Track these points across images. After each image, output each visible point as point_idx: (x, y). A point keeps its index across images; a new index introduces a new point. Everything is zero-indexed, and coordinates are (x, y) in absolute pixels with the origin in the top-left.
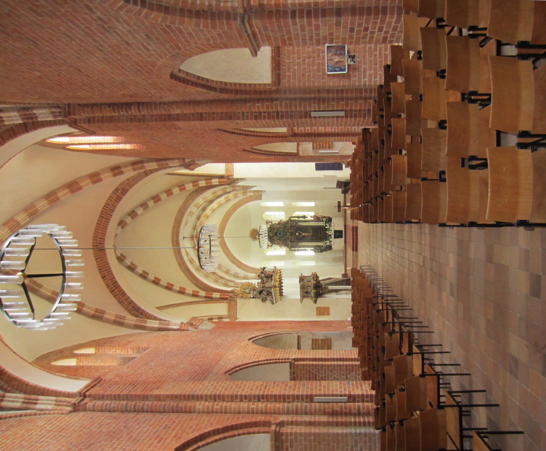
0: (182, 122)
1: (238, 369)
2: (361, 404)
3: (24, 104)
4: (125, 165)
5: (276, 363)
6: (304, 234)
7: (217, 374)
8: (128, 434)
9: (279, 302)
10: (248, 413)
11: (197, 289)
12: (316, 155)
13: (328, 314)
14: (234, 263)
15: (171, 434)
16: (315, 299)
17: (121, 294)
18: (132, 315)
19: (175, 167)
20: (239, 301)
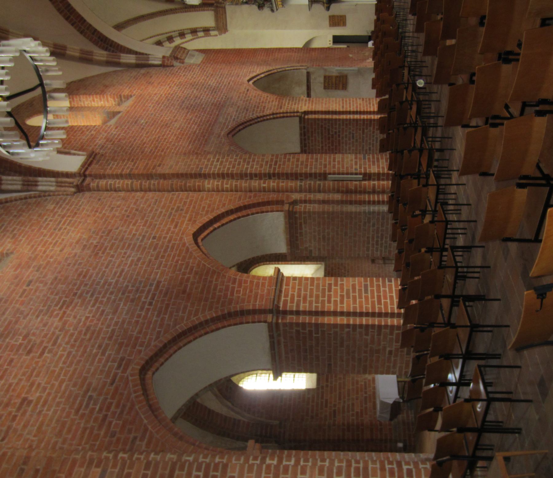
1: (241, 127)
2: (376, 182)
5: (283, 117)
7: (219, 136)
8: (143, 219)
9: (281, 9)
10: (260, 191)
13: (344, 24)
15: (185, 217)
16: (327, 5)
18: (99, 47)
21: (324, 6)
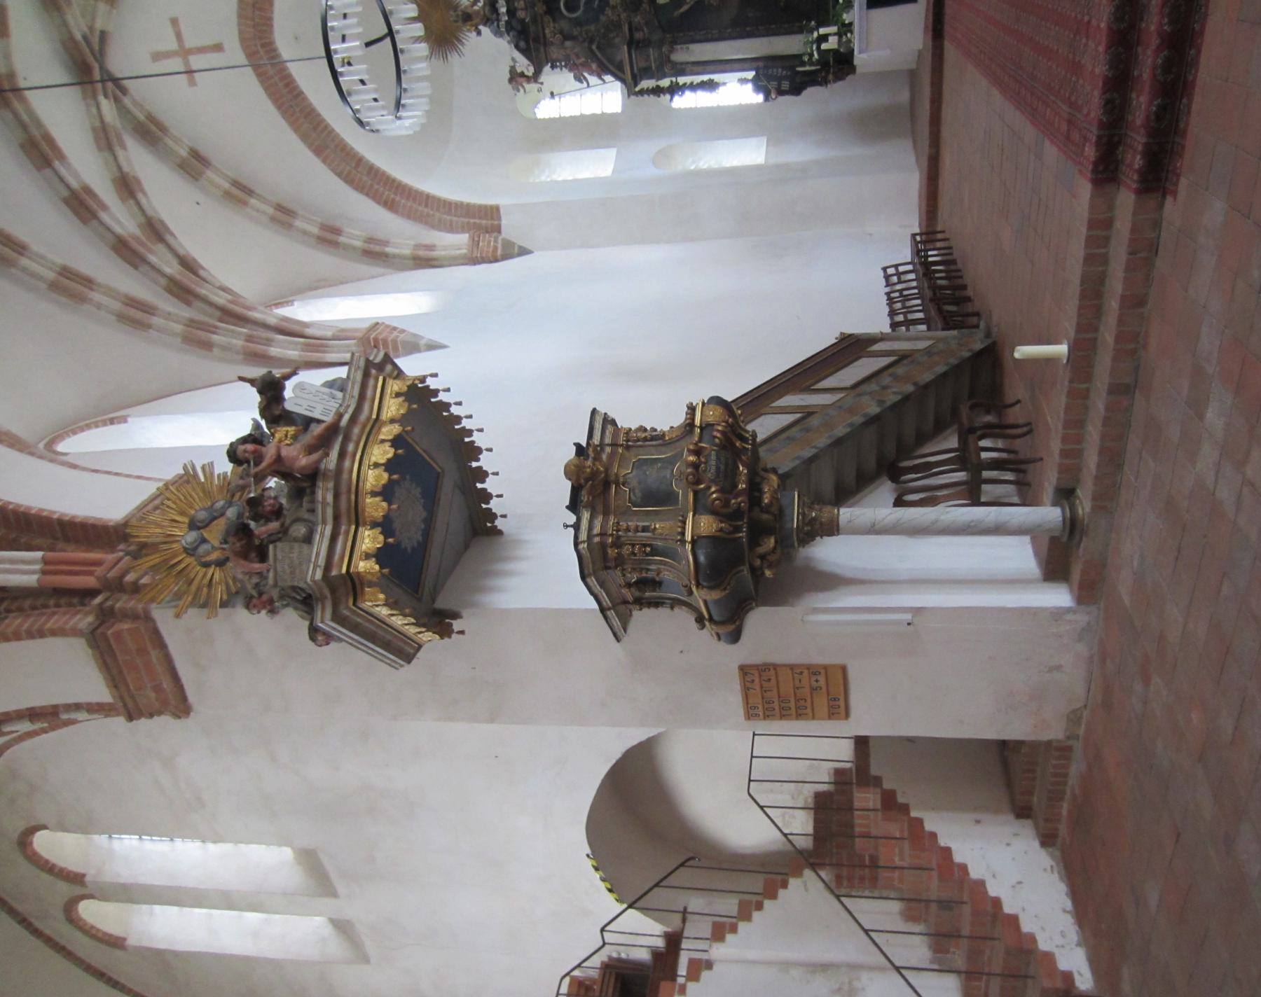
14: (360, 188)
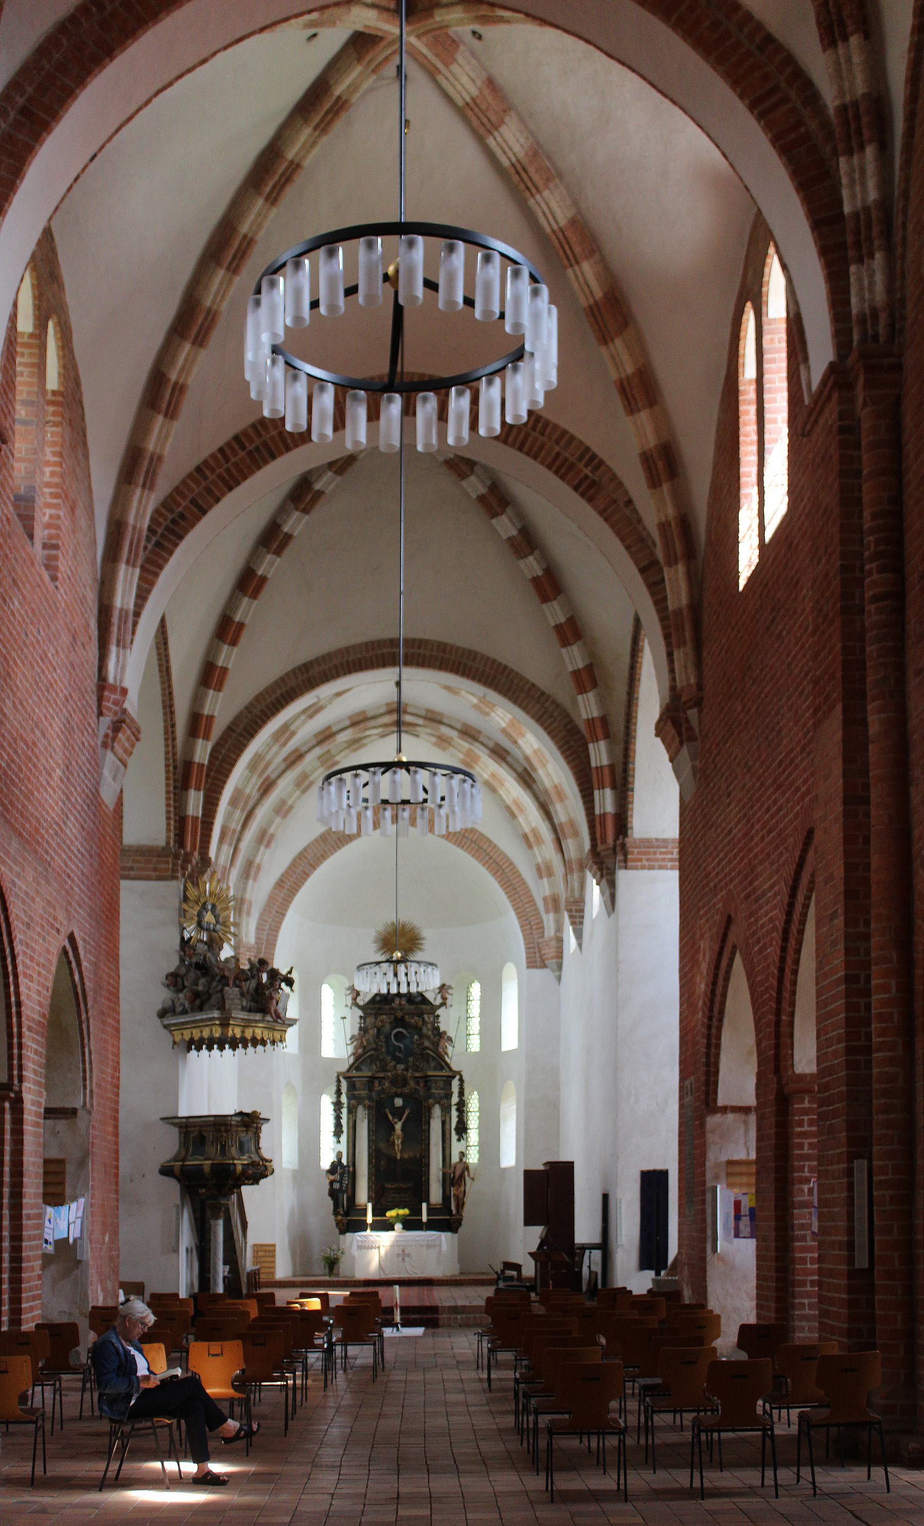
0: (839, 735)
3: (904, 225)
4: (681, 498)
5: (10, 1036)
6: (398, 1126)
11: (217, 731)
12: (709, 1175)
14: (294, 864)
16: (177, 1170)
17: (228, 470)
18: (157, 511)
19: (672, 671)
20: (171, 890)
21: (175, 1159)
